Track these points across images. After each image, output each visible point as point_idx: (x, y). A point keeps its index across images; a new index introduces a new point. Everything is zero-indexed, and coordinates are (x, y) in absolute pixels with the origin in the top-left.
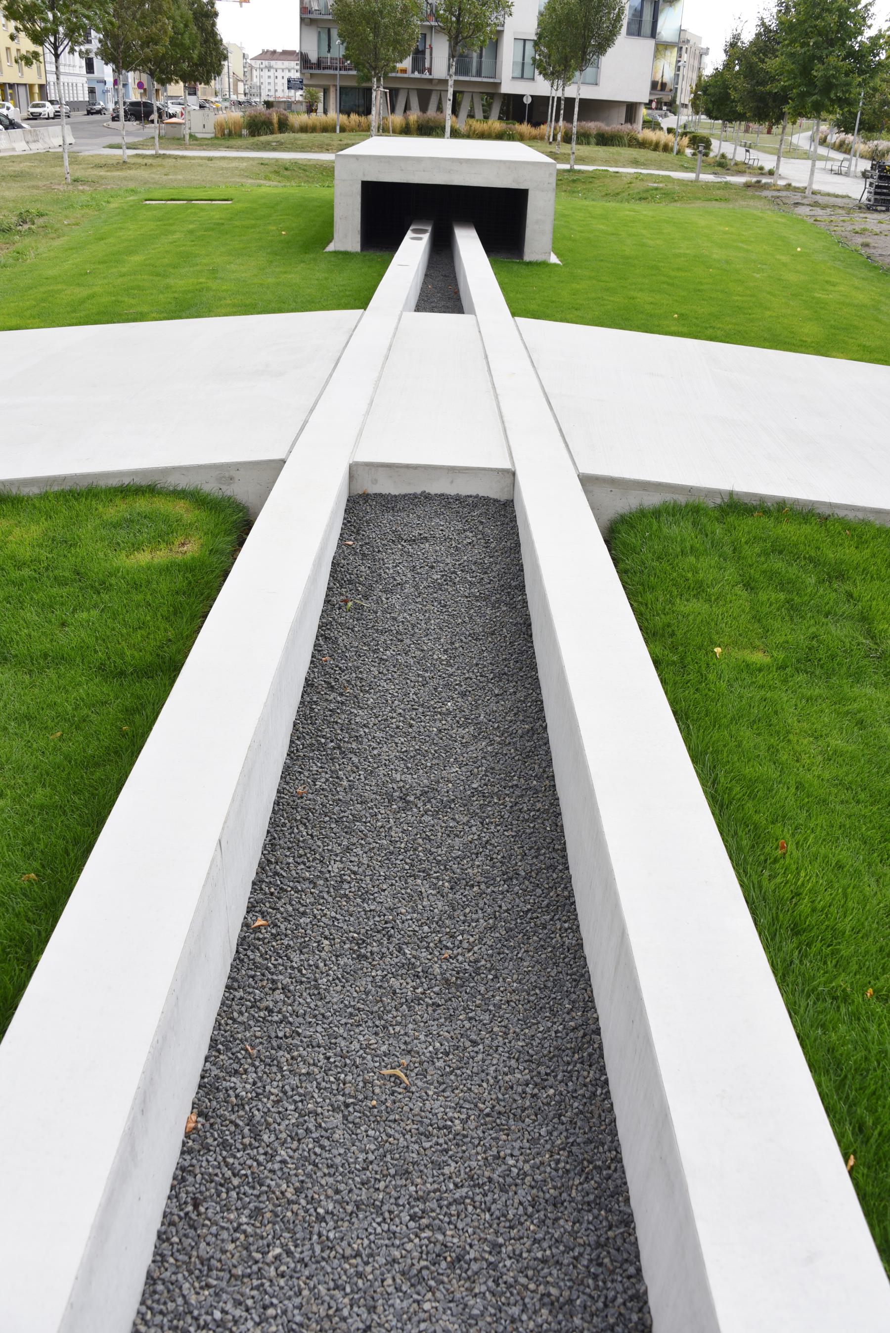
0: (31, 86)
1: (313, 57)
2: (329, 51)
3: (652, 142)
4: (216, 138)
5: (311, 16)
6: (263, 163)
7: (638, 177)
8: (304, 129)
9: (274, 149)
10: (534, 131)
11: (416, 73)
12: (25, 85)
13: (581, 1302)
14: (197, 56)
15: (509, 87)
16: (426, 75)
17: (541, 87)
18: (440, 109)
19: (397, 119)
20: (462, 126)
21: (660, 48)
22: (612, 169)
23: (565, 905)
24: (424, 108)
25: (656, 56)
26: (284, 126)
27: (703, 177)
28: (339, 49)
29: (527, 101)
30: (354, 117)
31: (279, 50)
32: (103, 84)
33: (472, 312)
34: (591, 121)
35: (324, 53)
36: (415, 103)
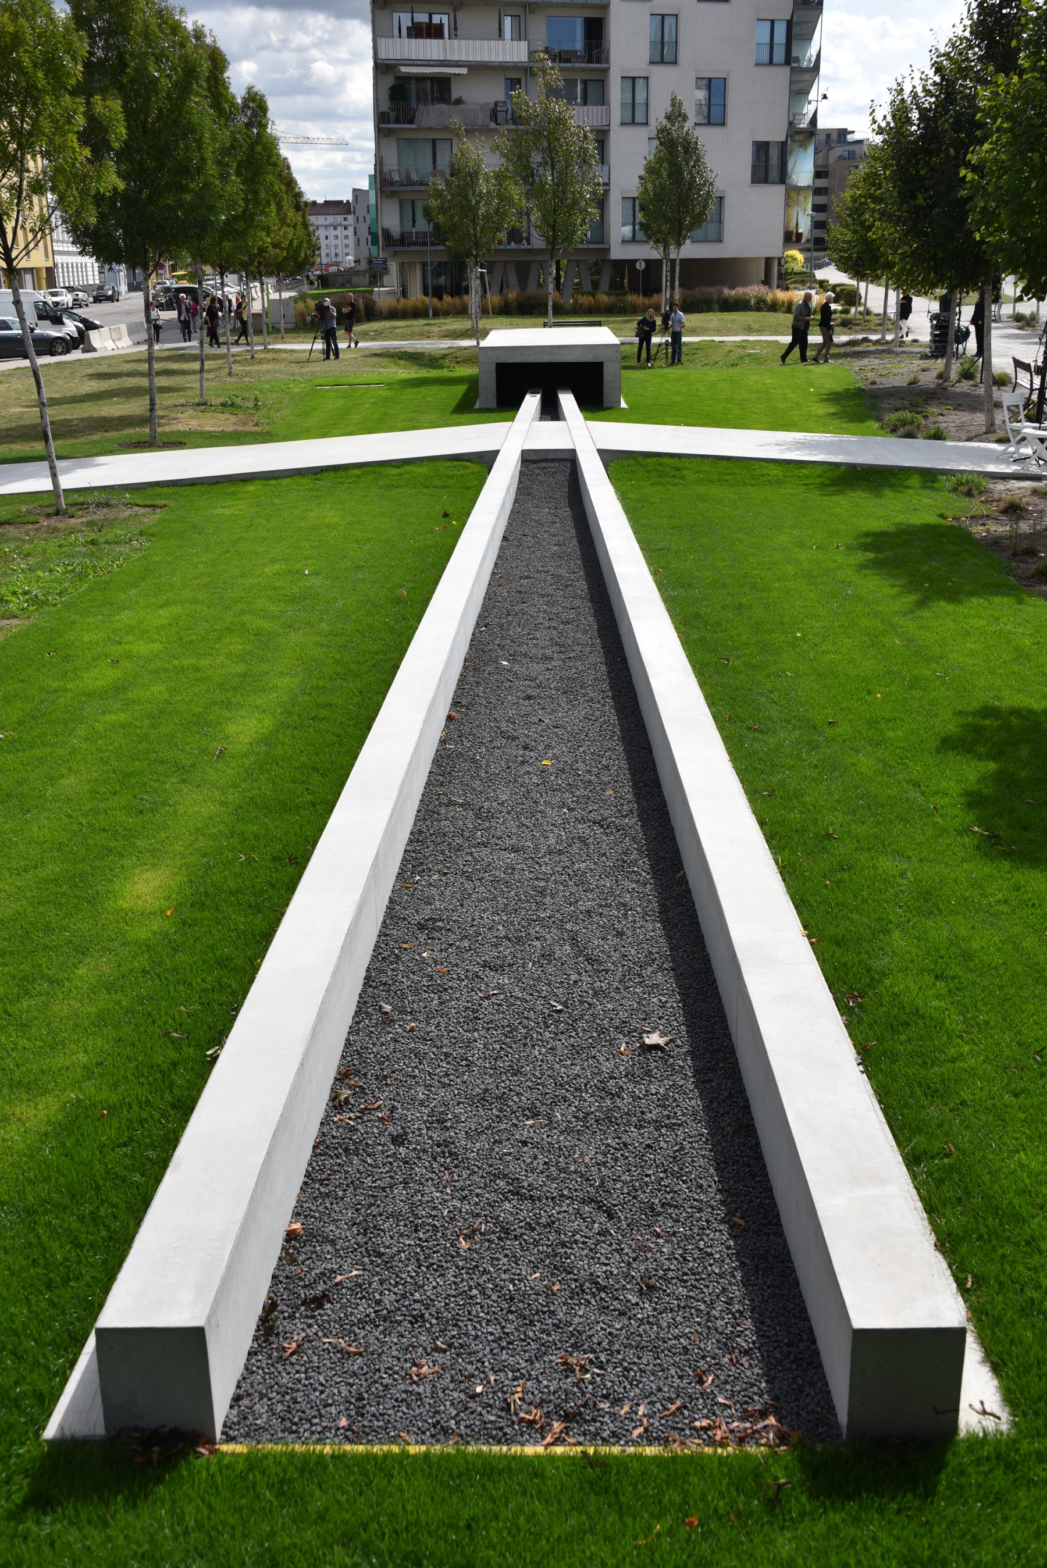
0: (38, 269)
2: (414, 225)
3: (783, 302)
5: (392, 188)
7: (742, 345)
11: (513, 244)
12: (32, 269)
13: (775, 1435)
15: (618, 252)
16: (525, 245)
17: (645, 252)
21: (792, 195)
22: (717, 339)
25: (788, 204)
29: (641, 266)
30: (447, 298)
31: (320, 200)
33: (565, 420)
34: (711, 286)
35: (408, 227)
36: (513, 278)
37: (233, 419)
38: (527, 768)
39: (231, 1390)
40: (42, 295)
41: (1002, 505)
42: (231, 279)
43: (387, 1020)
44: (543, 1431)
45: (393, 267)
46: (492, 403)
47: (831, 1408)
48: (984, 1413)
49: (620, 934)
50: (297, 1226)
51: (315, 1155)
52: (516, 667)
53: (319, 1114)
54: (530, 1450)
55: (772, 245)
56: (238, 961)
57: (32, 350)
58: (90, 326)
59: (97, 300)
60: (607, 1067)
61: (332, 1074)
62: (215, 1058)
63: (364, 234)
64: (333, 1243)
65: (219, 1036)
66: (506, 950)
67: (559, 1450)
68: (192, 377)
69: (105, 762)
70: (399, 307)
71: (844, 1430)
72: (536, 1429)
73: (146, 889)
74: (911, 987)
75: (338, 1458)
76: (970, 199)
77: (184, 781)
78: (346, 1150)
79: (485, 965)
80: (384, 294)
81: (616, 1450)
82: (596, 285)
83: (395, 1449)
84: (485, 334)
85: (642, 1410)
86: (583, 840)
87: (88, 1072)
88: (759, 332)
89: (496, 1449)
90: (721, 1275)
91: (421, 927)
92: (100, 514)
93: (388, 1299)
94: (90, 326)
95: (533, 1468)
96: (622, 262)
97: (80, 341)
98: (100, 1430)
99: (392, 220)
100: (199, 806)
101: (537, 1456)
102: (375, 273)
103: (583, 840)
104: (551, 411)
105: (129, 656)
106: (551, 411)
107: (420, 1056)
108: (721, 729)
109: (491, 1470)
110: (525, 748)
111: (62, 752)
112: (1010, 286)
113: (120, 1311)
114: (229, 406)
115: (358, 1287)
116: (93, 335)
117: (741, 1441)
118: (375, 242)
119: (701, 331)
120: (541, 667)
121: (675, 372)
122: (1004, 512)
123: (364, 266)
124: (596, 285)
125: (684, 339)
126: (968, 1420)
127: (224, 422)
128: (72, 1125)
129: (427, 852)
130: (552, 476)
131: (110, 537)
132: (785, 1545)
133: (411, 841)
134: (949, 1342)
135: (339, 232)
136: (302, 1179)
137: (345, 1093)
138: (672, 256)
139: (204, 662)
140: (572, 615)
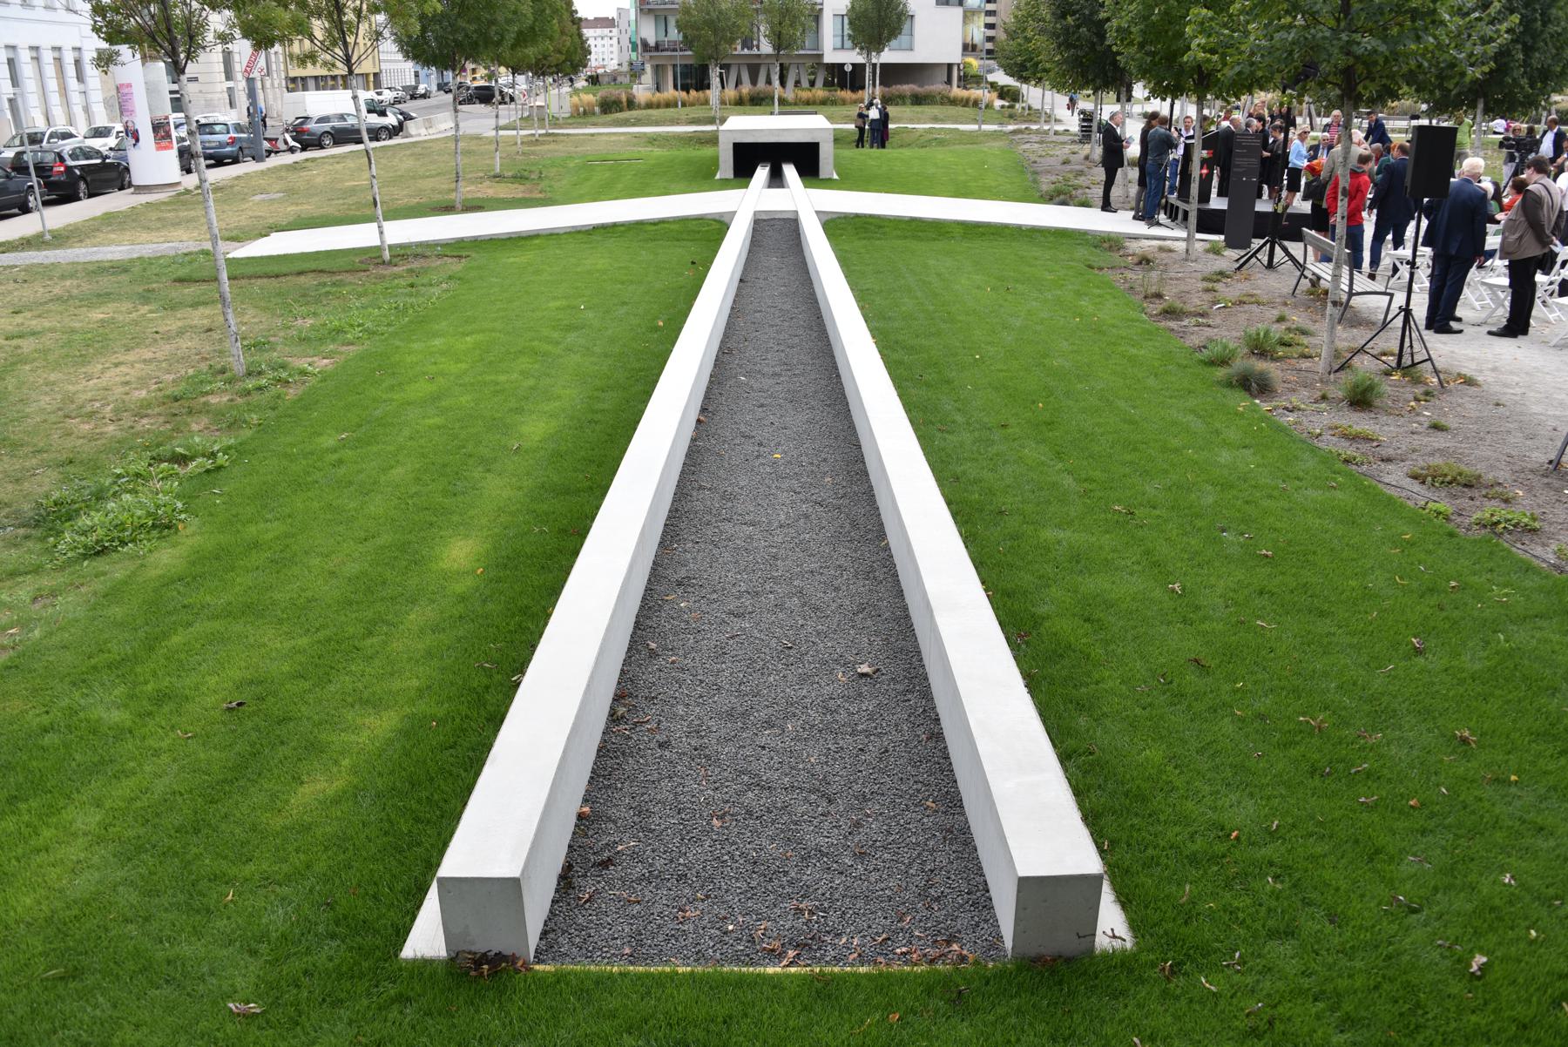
1: (652, 42)
4: (572, 116)
6: (636, 136)
8: (649, 106)
9: (634, 125)
10: (854, 96)
14: (562, 55)
15: (830, 57)
18: (769, 82)
19: (731, 92)
20: (790, 94)
23: (878, 533)
24: (754, 82)
26: (631, 104)
27: (984, 127)
28: (674, 35)
29: (848, 69)
30: (693, 93)
32: (1502, 314)
35: (662, 37)
36: (745, 77)
37: (522, 188)
38: (761, 460)
39: (540, 926)
40: (371, 94)
41: (1136, 260)
42: (521, 79)
43: (653, 654)
44: (781, 956)
45: (648, 68)
46: (730, 175)
47: (1000, 937)
48: (1114, 937)
49: (837, 589)
50: (586, 809)
51: (598, 756)
52: (752, 382)
53: (601, 726)
54: (770, 970)
55: (953, 55)
56: (534, 609)
57: (365, 137)
58: (408, 118)
59: (413, 97)
60: (827, 690)
61: (611, 696)
62: (517, 685)
63: (626, 43)
64: (615, 822)
65: (522, 669)
66: (747, 601)
67: (793, 970)
68: (270, 97)
69: (423, 455)
70: (655, 99)
71: (1009, 952)
72: (774, 955)
73: (460, 553)
74: (1065, 627)
75: (623, 975)
76: (1108, 19)
77: (489, 471)
78: (623, 753)
79: (731, 613)
80: (642, 91)
81: (836, 969)
82: (812, 83)
83: (667, 969)
84: (723, 121)
85: (856, 942)
86: (807, 516)
87: (421, 692)
88: (942, 121)
89: (744, 969)
90: (918, 844)
91: (679, 584)
92: (416, 265)
93: (659, 864)
94: (408, 118)
95: (775, 983)
96: (833, 65)
97: (396, 131)
98: (443, 953)
99: (649, 33)
100: (499, 490)
101: (776, 974)
102: (635, 73)
103: (807, 516)
104: (776, 179)
105: (442, 374)
106: (776, 179)
107: (680, 683)
108: (916, 430)
109: (741, 982)
110: (760, 444)
111: (391, 448)
112: (1139, 90)
113: (455, 863)
114: (519, 178)
115: (635, 855)
116: (409, 123)
117: (932, 961)
118: (635, 48)
119: (904, 121)
120: (771, 382)
121: (876, 152)
122: (1140, 263)
123: (625, 68)
124: (812, 83)
125: (891, 126)
126: (1102, 942)
127: (517, 191)
128: (411, 731)
129: (682, 526)
130: (777, 234)
131: (425, 281)
132: (965, 1031)
133: (669, 518)
134: (1086, 886)
135: (606, 41)
136: (588, 774)
137: (621, 710)
138: (874, 61)
139: (502, 378)
140: (796, 340)
